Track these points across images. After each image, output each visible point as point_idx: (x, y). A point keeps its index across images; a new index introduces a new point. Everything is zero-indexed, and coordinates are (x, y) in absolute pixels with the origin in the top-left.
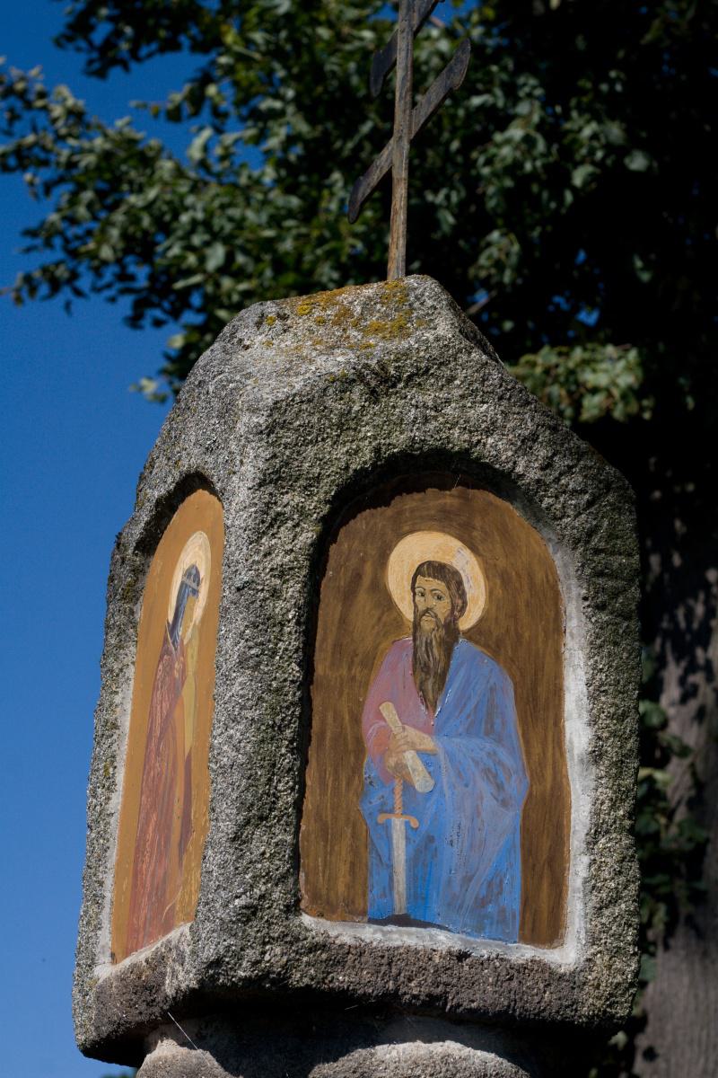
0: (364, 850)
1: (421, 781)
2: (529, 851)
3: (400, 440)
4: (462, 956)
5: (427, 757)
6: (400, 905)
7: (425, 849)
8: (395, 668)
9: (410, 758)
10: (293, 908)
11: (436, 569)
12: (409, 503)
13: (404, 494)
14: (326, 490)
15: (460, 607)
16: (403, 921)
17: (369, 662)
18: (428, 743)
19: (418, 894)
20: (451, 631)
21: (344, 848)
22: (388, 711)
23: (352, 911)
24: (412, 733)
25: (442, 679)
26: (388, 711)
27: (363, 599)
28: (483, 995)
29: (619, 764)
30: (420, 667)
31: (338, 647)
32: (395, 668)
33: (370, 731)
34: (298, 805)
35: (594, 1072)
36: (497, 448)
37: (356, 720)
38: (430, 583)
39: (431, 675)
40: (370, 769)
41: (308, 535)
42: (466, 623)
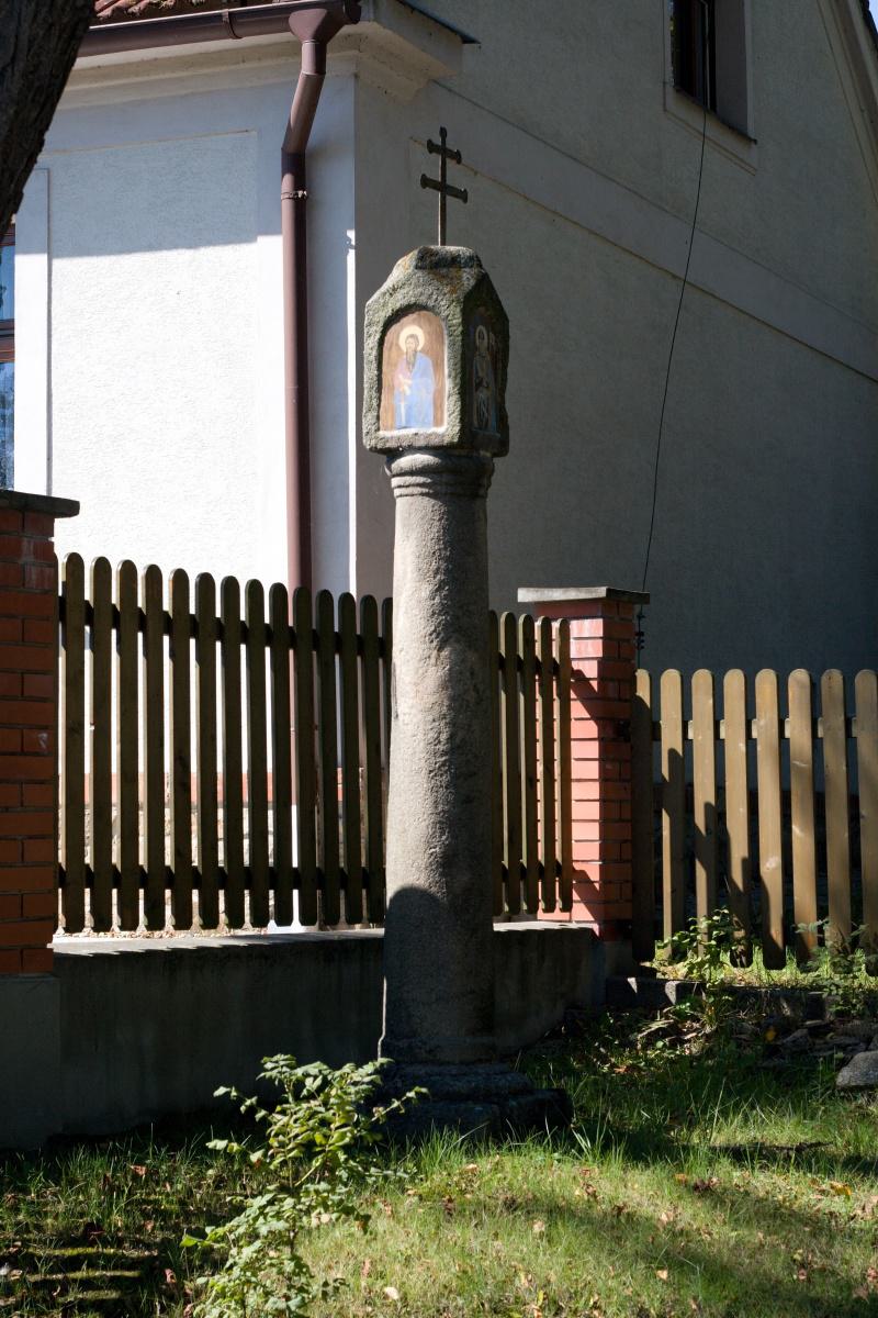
0: (394, 410)
1: (408, 392)
2: (435, 404)
3: (398, 305)
4: (416, 434)
5: (410, 387)
6: (404, 424)
7: (409, 408)
8: (402, 365)
9: (406, 388)
10: (378, 429)
11: (412, 336)
12: (404, 320)
13: (53, 539)
14: (381, 324)
15: (417, 345)
16: (405, 427)
17: (396, 365)
18: (410, 382)
19: (408, 421)
20: (416, 351)
21: (390, 414)
22: (401, 376)
23: (392, 428)
24: (406, 381)
25: (413, 365)
26: (401, 376)
27: (394, 349)
28: (422, 443)
29: (455, 377)
30: (408, 363)
31: (388, 363)
32: (402, 365)
33: (396, 382)
34: (379, 405)
35: (171, 394)
36: (423, 300)
37: (392, 380)
38: (410, 340)
39: (411, 364)
40: (396, 392)
41: (378, 336)
42: (419, 348)
